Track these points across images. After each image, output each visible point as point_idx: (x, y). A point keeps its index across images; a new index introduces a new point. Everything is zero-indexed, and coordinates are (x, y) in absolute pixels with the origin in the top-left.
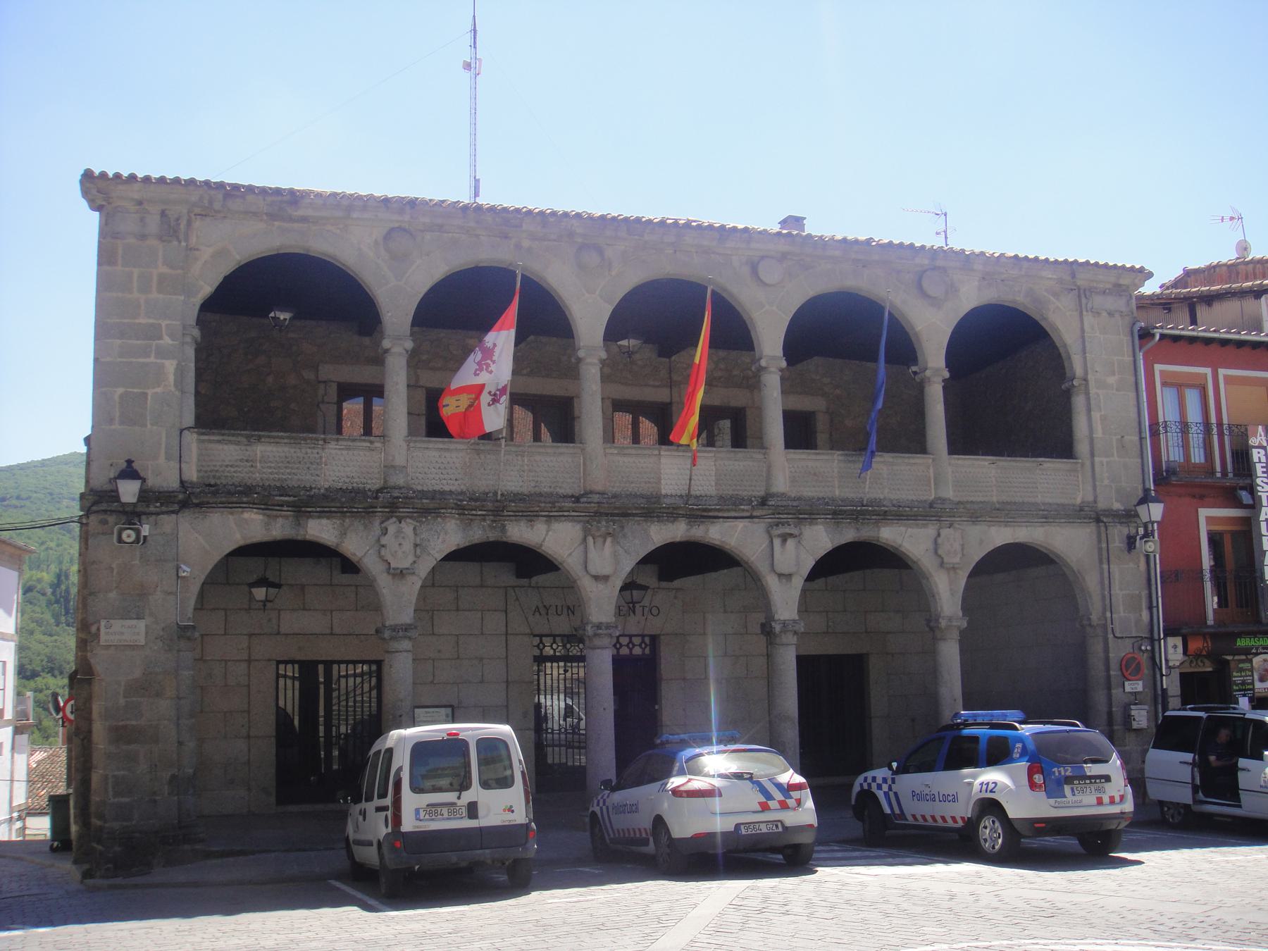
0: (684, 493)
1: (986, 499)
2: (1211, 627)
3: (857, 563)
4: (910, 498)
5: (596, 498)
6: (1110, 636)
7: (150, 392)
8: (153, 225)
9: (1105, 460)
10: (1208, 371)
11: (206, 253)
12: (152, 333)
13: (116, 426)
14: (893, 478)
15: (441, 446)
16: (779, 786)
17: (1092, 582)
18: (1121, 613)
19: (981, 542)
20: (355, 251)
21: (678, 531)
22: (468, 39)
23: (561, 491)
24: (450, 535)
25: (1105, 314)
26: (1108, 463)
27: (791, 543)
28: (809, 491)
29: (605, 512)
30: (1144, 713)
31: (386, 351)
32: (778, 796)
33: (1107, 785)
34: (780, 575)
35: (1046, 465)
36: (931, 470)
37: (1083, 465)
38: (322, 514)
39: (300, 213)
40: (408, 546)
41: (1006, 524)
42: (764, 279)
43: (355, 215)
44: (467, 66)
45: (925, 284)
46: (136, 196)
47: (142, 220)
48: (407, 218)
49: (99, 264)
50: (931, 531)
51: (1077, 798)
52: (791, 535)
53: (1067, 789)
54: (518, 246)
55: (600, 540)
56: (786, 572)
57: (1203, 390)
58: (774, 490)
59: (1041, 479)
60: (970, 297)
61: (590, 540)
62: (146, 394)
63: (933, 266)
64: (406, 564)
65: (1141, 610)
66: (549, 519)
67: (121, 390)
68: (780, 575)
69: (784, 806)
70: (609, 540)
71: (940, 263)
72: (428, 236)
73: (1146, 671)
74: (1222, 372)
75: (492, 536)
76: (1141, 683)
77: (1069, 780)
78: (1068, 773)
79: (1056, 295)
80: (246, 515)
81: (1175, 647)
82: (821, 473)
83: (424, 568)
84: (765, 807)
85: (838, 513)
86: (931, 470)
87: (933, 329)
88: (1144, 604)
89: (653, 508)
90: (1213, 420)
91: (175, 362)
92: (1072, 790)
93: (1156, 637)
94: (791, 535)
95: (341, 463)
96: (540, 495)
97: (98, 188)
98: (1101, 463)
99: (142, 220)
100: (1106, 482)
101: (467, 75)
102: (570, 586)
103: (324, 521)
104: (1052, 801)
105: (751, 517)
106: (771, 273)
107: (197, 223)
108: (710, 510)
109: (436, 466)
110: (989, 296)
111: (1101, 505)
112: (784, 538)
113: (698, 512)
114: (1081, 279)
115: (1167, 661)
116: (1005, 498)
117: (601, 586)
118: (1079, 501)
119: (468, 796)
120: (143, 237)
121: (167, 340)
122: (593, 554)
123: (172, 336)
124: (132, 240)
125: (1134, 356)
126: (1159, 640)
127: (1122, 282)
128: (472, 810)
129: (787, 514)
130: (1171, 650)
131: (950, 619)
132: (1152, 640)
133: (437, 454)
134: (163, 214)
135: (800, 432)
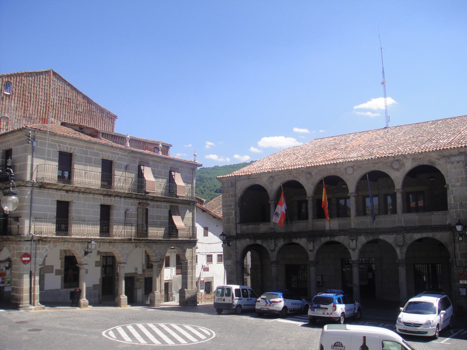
9: (454, 210)
11: (239, 188)
12: (230, 206)
14: (386, 221)
16: (270, 302)
17: (450, 249)
19: (411, 238)
20: (263, 182)
21: (328, 239)
22: (382, 75)
25: (456, 163)
26: (456, 211)
27: (354, 241)
28: (361, 227)
29: (312, 235)
30: (465, 291)
34: (352, 249)
38: (259, 239)
39: (252, 177)
40: (273, 245)
45: (393, 166)
50: (394, 236)
54: (293, 176)
59: (436, 218)
60: (409, 166)
63: (397, 160)
64: (273, 248)
66: (300, 238)
68: (352, 249)
69: (270, 305)
71: (397, 159)
72: (276, 177)
77: (316, 308)
79: (439, 159)
82: (366, 222)
83: (277, 249)
84: (266, 305)
87: (398, 177)
89: (323, 233)
98: (453, 212)
100: (455, 217)
106: (350, 171)
107: (237, 182)
110: (415, 164)
112: (352, 240)
114: (446, 154)
116: (420, 224)
118: (447, 223)
119: (223, 298)
120: (228, 187)
121: (233, 207)
122: (309, 245)
124: (226, 188)
128: (224, 300)
129: (354, 233)
135: (362, 211)
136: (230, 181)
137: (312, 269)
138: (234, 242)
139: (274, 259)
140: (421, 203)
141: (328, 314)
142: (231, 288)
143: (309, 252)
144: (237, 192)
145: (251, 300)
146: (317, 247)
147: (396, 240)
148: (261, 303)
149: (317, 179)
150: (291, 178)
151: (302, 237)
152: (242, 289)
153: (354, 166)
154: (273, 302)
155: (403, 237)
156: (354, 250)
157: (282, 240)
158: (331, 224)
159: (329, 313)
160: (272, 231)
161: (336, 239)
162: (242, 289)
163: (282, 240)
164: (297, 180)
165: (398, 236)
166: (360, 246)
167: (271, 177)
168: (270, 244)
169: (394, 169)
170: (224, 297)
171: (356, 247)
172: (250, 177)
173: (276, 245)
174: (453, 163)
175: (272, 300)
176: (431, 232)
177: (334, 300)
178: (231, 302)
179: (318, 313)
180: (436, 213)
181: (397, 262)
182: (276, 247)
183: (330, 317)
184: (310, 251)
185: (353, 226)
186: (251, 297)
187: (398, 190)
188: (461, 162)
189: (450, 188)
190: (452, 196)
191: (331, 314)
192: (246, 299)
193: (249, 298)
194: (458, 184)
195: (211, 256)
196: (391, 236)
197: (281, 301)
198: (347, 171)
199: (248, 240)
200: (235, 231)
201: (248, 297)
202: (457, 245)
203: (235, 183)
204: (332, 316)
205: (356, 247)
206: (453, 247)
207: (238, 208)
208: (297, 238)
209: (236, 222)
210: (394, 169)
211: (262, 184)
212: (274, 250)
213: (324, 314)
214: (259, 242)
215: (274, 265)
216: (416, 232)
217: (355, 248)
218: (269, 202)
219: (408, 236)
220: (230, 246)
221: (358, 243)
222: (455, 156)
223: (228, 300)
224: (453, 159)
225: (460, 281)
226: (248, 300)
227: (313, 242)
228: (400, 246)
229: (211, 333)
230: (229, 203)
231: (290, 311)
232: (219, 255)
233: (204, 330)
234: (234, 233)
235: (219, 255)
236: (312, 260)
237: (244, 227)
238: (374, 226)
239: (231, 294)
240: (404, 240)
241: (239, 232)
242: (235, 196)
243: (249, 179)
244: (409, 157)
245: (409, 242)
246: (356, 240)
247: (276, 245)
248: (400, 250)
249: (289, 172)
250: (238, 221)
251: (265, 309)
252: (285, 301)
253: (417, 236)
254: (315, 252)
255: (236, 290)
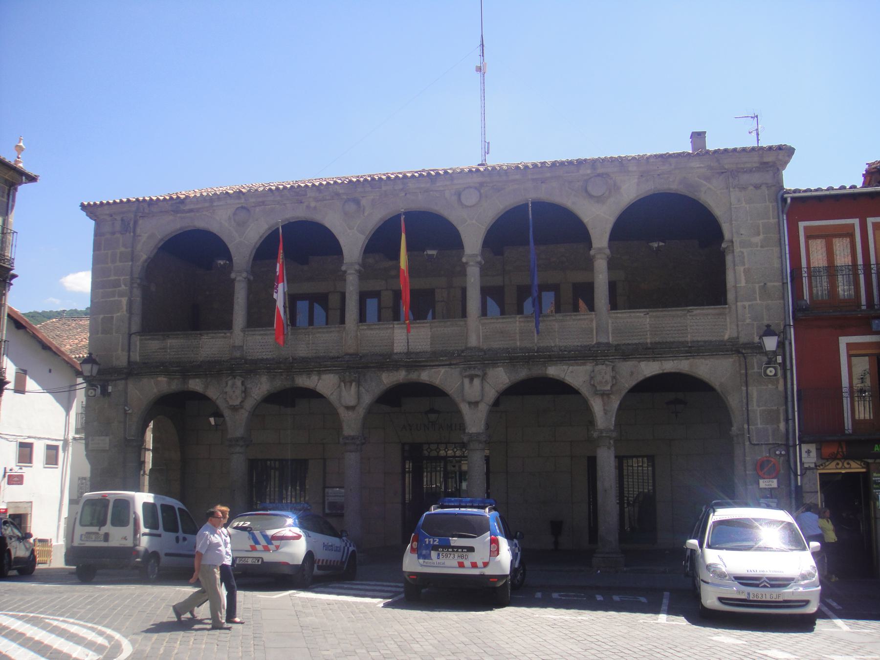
0: (406, 351)
1: (641, 341)
2: (849, 435)
3: (538, 393)
4: (576, 344)
5: (347, 358)
6: (747, 443)
7: (115, 315)
8: (118, 226)
9: (747, 304)
10: (856, 222)
12: (116, 284)
13: (100, 335)
15: (262, 332)
16: (265, 537)
17: (734, 401)
18: (759, 424)
19: (632, 373)
20: (219, 223)
21: (401, 376)
22: (478, 51)
23: (331, 355)
24: (262, 387)
25: (751, 188)
27: (477, 382)
28: (496, 344)
29: (354, 366)
31: (345, 272)
32: (263, 542)
33: (470, 554)
34: (470, 403)
35: (695, 312)
36: (594, 322)
37: (730, 308)
39: (187, 208)
40: (238, 392)
41: (654, 359)
42: (467, 204)
43: (215, 204)
44: (479, 69)
45: (589, 188)
46: (108, 212)
47: (113, 224)
48: (243, 201)
49: (94, 250)
50: (589, 367)
51: (441, 561)
52: (477, 376)
53: (434, 554)
54: (308, 207)
55: (349, 384)
56: (473, 400)
57: (852, 236)
58: (469, 345)
59: (697, 323)
60: (630, 191)
61: (343, 384)
62: (112, 317)
64: (237, 402)
65: (779, 422)
66: (320, 373)
67: (102, 316)
68: (470, 403)
69: (266, 549)
70: (354, 384)
71: (600, 170)
72: (257, 209)
73: (782, 471)
74: (870, 221)
75: (288, 384)
76: (775, 481)
77: (435, 548)
78: (436, 543)
79: (708, 179)
80: (159, 379)
81: (808, 452)
82: (515, 331)
83: (249, 404)
84: (253, 549)
85: (512, 358)
86: (594, 322)
88: (782, 417)
89: (386, 361)
90: (860, 261)
91: (126, 298)
92: (439, 555)
93: (791, 443)
94: (477, 376)
95: (210, 346)
96: (318, 357)
97: (90, 209)
99: (113, 224)
100: (748, 321)
101: (478, 75)
102: (334, 412)
103: (197, 380)
104: (421, 561)
105: (450, 365)
106: (470, 198)
107: (140, 222)
108: (419, 362)
109: (260, 344)
110: (648, 188)
111: (743, 339)
112: (471, 378)
113: (413, 361)
115: (802, 464)
116: (657, 339)
117: (350, 413)
118: (726, 337)
120: (113, 233)
121: (123, 287)
122: (344, 393)
123: (125, 285)
125: (779, 219)
126: (795, 446)
127: (766, 160)
128: (106, 537)
129: (478, 361)
130: (804, 455)
131: (601, 431)
132: (787, 446)
133: (260, 337)
134: (122, 220)
136: (119, 218)
137: (352, 459)
138: (121, 384)
139: (239, 432)
140: (269, 462)
141: (474, 565)
142: (133, 498)
143: (342, 411)
144: (139, 247)
145: (185, 539)
146: (367, 399)
147: (592, 378)
148: (223, 542)
149: (375, 217)
150: (299, 213)
151: (325, 372)
152: (163, 506)
153: (482, 184)
154: (275, 538)
155: (613, 369)
156: (474, 404)
157: (264, 379)
158: (405, 337)
159: (480, 564)
160: (238, 354)
161: (425, 376)
162: (163, 506)
163: (264, 379)
164: (318, 218)
165: (600, 367)
166: (491, 394)
167: (243, 208)
168: (228, 389)
169: (591, 196)
170: (108, 528)
171: (483, 395)
172: (182, 207)
173: (246, 392)
174: (743, 188)
175: (271, 532)
176: (687, 358)
177: (491, 523)
178: (129, 543)
179: (445, 564)
180: (697, 311)
181: (595, 435)
182: (245, 398)
183: (482, 576)
184: (348, 408)
185: (473, 342)
186: (184, 532)
187: (600, 250)
188: (764, 188)
189: (737, 249)
190: (742, 269)
191: (486, 565)
192: (172, 535)
193: (181, 534)
194: (757, 240)
195: (30, 446)
196: (581, 368)
197: (298, 537)
198: (463, 197)
199: (162, 379)
200: (126, 353)
201: (176, 531)
202: (754, 391)
203: (136, 223)
204: (488, 571)
205: (483, 395)
206: (744, 395)
207: (137, 292)
208: (309, 372)
209: (129, 328)
210: (591, 196)
211: (214, 228)
212: (241, 406)
213: (461, 565)
214: (195, 385)
215: (238, 449)
216: (648, 359)
217: (478, 399)
218: (233, 276)
219: (625, 367)
220: (109, 394)
221: (487, 387)
222: (750, 171)
223: (118, 537)
224: (745, 178)
225: (761, 481)
226: (177, 539)
227: (359, 385)
228: (604, 395)
229: (109, 638)
230: (113, 278)
231: (319, 568)
232: (49, 447)
233: (74, 629)
234: (120, 359)
235: (49, 447)
236: (352, 434)
237: (154, 345)
238: (535, 342)
239: (132, 516)
240: (614, 377)
241: (136, 357)
242: (133, 258)
243: (176, 211)
244: (632, 168)
245: (628, 383)
246: (483, 378)
247: (246, 392)
248: (604, 405)
249: (297, 193)
250: (135, 328)
251: (250, 561)
252: (308, 536)
253: (650, 368)
254: (361, 411)
255: (145, 505)
